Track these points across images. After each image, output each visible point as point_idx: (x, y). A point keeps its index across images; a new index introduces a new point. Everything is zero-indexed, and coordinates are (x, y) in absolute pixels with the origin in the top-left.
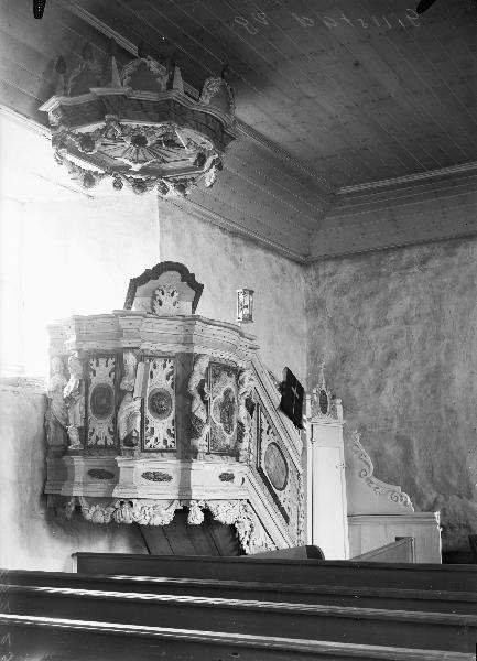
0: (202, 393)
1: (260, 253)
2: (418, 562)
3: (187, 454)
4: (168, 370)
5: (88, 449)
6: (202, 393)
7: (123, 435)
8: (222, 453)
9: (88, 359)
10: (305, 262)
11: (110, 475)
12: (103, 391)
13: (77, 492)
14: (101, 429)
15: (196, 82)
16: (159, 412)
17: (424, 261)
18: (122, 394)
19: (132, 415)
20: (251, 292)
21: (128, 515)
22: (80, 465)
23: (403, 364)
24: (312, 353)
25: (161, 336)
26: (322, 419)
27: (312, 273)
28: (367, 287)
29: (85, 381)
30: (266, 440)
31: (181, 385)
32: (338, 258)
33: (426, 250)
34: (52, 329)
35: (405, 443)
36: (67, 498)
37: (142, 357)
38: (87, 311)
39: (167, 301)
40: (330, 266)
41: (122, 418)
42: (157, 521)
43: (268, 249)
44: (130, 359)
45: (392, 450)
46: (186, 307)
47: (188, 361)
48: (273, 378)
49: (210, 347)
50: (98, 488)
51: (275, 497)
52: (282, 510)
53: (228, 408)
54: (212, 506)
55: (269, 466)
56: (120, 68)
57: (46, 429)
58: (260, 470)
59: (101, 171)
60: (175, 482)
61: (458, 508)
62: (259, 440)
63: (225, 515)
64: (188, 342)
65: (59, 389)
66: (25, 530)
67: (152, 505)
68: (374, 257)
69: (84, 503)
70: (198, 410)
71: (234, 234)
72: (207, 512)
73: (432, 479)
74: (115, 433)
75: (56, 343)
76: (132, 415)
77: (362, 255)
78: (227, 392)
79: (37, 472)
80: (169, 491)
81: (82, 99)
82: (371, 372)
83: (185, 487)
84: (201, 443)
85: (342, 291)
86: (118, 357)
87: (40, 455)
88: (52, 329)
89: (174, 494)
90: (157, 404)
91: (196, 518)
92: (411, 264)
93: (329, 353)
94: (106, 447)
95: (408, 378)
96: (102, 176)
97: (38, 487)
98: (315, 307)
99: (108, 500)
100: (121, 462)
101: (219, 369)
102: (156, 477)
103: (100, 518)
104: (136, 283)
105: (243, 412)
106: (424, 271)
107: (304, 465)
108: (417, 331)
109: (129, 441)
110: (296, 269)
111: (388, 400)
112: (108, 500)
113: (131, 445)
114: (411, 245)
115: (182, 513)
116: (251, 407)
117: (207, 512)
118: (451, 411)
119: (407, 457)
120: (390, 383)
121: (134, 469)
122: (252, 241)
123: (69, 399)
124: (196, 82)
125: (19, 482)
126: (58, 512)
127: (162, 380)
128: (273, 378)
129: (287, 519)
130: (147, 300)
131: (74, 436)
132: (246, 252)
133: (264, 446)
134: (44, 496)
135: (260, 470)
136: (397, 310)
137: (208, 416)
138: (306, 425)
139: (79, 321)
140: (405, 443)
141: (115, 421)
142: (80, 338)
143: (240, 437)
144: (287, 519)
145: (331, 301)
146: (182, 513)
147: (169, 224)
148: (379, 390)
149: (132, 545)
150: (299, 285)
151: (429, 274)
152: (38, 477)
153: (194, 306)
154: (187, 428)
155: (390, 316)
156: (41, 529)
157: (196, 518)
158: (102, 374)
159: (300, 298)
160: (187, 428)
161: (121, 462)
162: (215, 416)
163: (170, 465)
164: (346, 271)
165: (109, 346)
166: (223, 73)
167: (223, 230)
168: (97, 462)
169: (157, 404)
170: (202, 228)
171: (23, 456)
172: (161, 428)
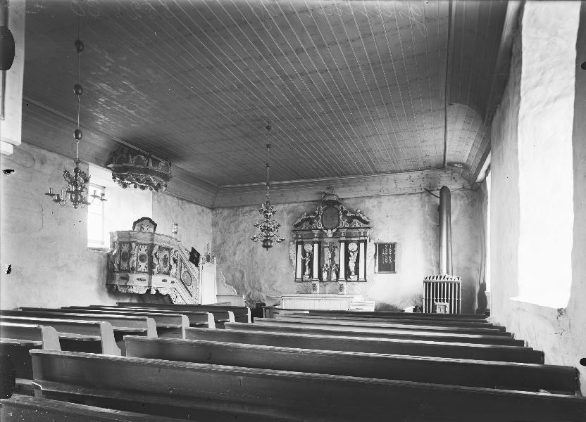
0: (156, 256)
1: (193, 205)
2: (554, 363)
3: (151, 273)
4: (146, 248)
5: (120, 271)
6: (156, 256)
7: (131, 267)
8: (165, 273)
9: (121, 244)
10: (212, 208)
11: (127, 279)
12: (125, 254)
13: (117, 283)
14: (125, 265)
15: (156, 162)
16: (142, 261)
17: (251, 211)
18: (131, 255)
19: (134, 261)
20: (177, 225)
21: (131, 290)
22: (118, 275)
23: (242, 246)
24: (214, 240)
25: (143, 237)
26: (207, 264)
27: (214, 212)
28: (233, 218)
29: (120, 250)
30: (183, 270)
31: (150, 252)
32: (223, 208)
33: (251, 208)
34: (111, 233)
35: (242, 273)
36: (114, 285)
37: (137, 244)
38: (121, 230)
39: (145, 228)
40: (221, 210)
41: (131, 262)
42: (141, 293)
43: (196, 204)
44: (134, 245)
45: (238, 275)
46: (152, 230)
47: (152, 246)
48: (186, 250)
49: (159, 242)
50: (123, 283)
51: (186, 288)
52: (189, 292)
53: (166, 260)
54: (159, 289)
55: (186, 278)
56: (132, 157)
57: (108, 264)
58: (181, 279)
59: (129, 182)
60: (147, 281)
61: (257, 295)
62: (181, 270)
63: (163, 292)
64: (152, 240)
65: (112, 252)
66: (100, 294)
67: (139, 287)
68: (235, 209)
69: (119, 287)
70: (155, 261)
71: (182, 199)
72: (157, 291)
73: (250, 285)
74: (128, 266)
75: (112, 238)
76: (134, 261)
77: (232, 207)
78: (165, 256)
79: (428, 217)
80: (146, 284)
81: (120, 166)
82: (232, 248)
83: (150, 283)
84: (155, 270)
85: (224, 219)
86: (130, 244)
87: (106, 272)
88: (111, 233)
89: (147, 285)
90: (142, 258)
91: (153, 292)
92: (247, 212)
93: (219, 241)
94: (126, 270)
95: (244, 251)
96: (129, 184)
97: (105, 281)
98: (215, 224)
99: (125, 286)
100: (130, 275)
101: (161, 249)
102: (141, 280)
103: (123, 291)
104: (135, 223)
105: (172, 262)
106: (250, 215)
107: (199, 278)
108: (248, 235)
109: (133, 269)
110: (208, 210)
111: (237, 258)
112: (125, 286)
113: (132, 270)
114: (247, 206)
115: (149, 291)
116: (175, 261)
117: (157, 291)
118: (256, 263)
119: (243, 277)
120: (238, 253)
121: (134, 277)
122: (190, 202)
123: (115, 255)
124: (156, 162)
125: (99, 279)
126: (112, 290)
127: (143, 251)
128: (186, 250)
129: (192, 296)
130: (139, 227)
131: (116, 267)
132: (187, 205)
133: (182, 272)
134: (107, 285)
135: (181, 279)
136: (242, 226)
137: (159, 265)
138: (201, 266)
139: (118, 232)
140: (242, 273)
141: (128, 263)
142: (119, 238)
143: (170, 269)
144: (192, 296)
145: (220, 222)
146: (149, 291)
147: (156, 197)
148: (235, 254)
149: (138, 300)
150: (209, 216)
151: (252, 216)
152: (105, 279)
153: (155, 230)
154: (151, 266)
155: (239, 230)
156: (106, 295)
157: (153, 292)
158: (125, 248)
159: (210, 220)
160: (151, 266)
161: (130, 275)
162: (161, 263)
163: (145, 276)
164: (226, 212)
165: (127, 240)
166: (166, 159)
167: (177, 198)
168: (123, 275)
169: (142, 258)
170: (169, 198)
171: (100, 271)
172: (143, 266)
